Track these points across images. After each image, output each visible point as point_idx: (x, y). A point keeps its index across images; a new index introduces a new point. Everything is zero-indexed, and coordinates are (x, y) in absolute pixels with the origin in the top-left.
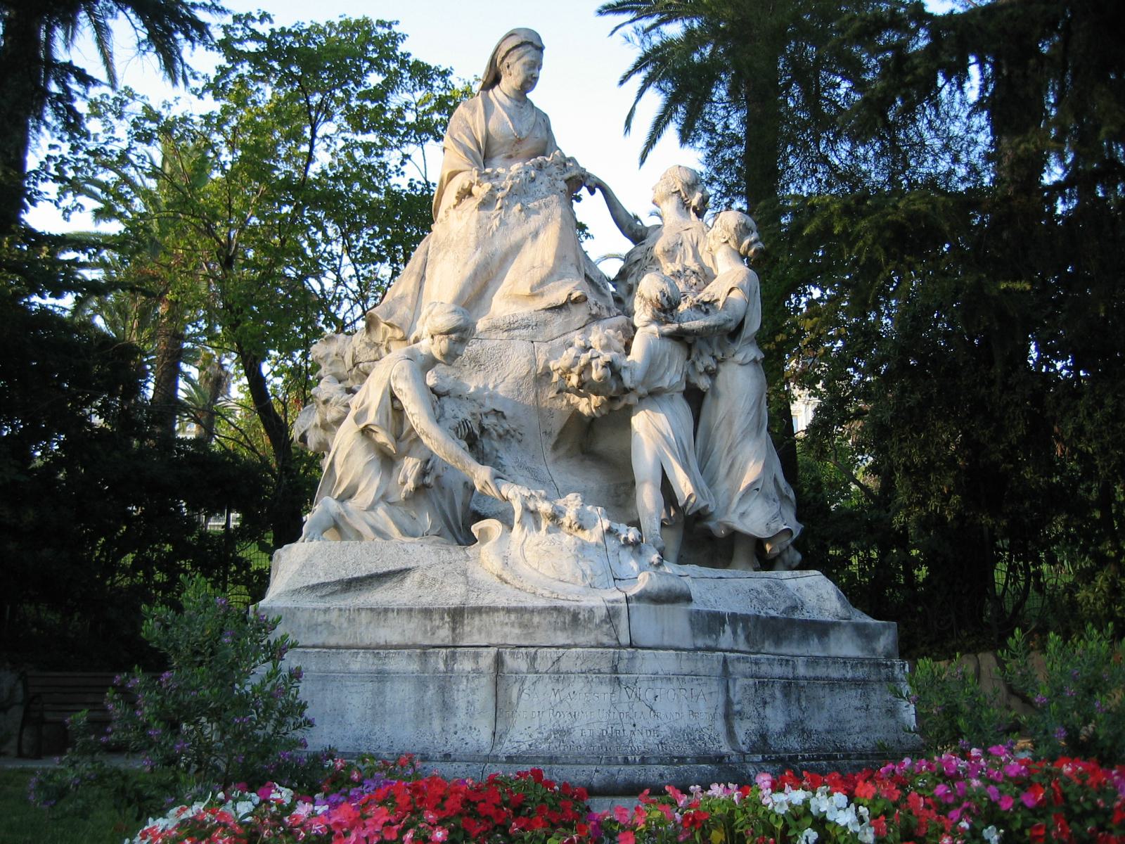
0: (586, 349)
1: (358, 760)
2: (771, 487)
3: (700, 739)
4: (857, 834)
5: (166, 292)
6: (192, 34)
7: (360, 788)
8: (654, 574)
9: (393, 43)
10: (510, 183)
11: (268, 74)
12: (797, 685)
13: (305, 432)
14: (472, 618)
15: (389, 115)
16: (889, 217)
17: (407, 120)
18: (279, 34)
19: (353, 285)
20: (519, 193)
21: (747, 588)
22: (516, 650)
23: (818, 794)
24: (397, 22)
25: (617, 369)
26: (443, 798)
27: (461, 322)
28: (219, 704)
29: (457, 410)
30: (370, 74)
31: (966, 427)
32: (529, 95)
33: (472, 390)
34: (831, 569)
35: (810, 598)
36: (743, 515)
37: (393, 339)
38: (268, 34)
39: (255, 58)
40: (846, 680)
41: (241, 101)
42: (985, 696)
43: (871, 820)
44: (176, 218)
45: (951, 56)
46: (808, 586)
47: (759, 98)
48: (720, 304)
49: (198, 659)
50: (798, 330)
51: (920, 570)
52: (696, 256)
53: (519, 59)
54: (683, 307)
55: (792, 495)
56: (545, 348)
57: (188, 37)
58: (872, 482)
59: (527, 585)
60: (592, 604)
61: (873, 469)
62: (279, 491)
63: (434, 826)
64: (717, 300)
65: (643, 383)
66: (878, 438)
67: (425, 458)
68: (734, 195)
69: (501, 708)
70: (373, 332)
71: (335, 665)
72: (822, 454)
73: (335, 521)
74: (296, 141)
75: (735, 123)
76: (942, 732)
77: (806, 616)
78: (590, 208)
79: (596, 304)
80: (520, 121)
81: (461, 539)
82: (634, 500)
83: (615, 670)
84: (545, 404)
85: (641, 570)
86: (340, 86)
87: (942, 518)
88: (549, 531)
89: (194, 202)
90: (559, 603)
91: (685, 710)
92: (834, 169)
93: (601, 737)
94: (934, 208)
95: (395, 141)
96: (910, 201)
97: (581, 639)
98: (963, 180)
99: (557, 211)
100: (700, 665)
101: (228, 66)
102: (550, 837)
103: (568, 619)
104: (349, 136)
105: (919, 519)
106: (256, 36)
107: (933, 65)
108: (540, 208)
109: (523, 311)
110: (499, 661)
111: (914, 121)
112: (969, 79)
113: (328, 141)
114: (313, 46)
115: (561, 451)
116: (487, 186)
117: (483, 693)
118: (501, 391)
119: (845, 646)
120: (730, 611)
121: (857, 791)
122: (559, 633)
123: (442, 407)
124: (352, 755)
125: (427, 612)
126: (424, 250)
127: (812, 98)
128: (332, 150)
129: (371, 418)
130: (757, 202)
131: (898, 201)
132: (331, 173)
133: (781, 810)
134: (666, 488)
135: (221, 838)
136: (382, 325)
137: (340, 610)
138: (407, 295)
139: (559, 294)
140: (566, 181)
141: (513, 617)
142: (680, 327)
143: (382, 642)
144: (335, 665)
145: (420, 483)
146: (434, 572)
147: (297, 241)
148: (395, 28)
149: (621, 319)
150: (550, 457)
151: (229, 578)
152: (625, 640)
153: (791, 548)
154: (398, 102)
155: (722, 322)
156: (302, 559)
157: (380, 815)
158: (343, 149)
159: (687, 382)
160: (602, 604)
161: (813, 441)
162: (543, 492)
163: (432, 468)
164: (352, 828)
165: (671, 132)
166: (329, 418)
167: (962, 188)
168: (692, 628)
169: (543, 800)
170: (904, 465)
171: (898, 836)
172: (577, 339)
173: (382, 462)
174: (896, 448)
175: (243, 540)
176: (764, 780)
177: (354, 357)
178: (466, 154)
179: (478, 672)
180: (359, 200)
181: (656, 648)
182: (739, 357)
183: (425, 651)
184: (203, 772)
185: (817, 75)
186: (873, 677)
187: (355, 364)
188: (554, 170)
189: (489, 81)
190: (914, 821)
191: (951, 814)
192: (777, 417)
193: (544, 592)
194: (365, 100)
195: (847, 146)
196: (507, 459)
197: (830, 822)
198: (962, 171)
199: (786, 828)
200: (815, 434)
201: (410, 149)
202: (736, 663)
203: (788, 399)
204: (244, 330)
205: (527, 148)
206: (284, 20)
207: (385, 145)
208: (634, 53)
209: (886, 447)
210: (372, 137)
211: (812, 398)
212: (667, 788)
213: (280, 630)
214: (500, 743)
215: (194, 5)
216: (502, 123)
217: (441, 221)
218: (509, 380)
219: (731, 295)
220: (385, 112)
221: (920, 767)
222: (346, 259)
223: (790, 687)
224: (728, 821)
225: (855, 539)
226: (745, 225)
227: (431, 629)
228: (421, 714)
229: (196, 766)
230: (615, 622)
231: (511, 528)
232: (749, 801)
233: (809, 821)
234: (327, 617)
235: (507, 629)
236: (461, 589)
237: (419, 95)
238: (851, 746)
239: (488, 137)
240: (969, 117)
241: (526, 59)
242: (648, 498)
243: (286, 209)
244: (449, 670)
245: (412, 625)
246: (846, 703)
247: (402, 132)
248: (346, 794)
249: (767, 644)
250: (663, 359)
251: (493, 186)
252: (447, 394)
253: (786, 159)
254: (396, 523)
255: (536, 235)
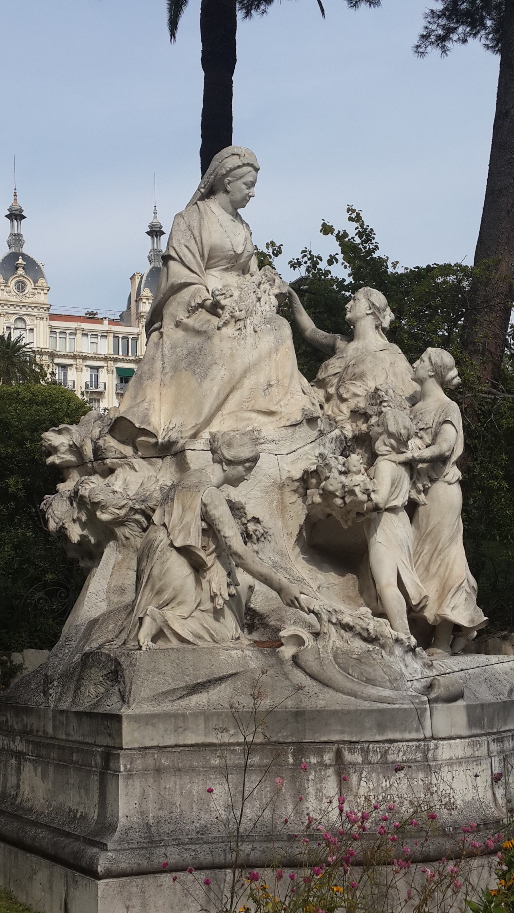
22: (352, 746)
71: (94, 749)
110: (339, 755)
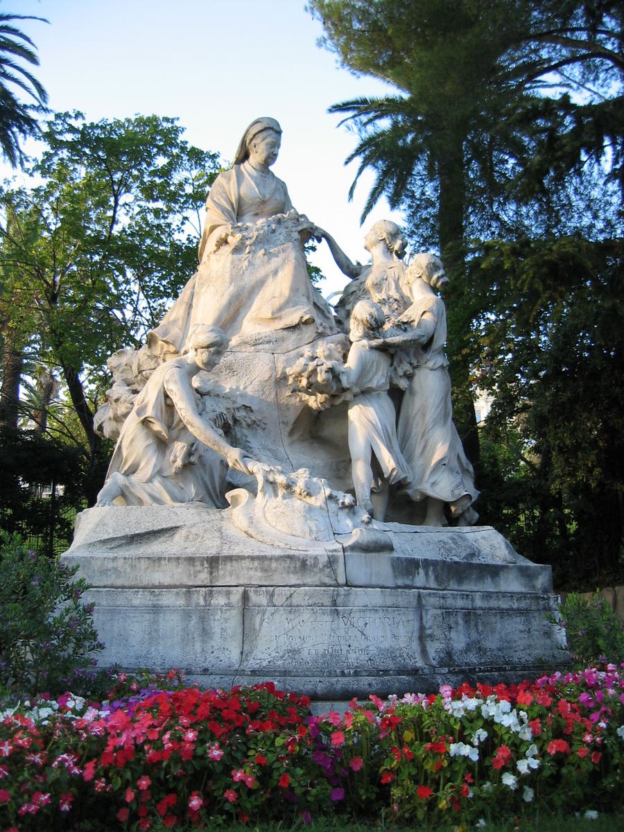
0: (313, 358)
1: (137, 674)
2: (455, 463)
3: (400, 656)
4: (518, 733)
5: (8, 320)
6: (24, 128)
7: (137, 696)
8: (364, 530)
9: (175, 134)
10: (256, 233)
11: (81, 157)
12: (475, 613)
13: (102, 423)
14: (225, 564)
15: (172, 188)
16: (546, 258)
17: (187, 192)
18: (89, 128)
19: (147, 315)
20: (262, 241)
21: (436, 540)
22: (258, 589)
23: (488, 702)
24: (178, 119)
25: (337, 373)
26: (197, 706)
27: (217, 339)
28: (27, 632)
29: (215, 406)
30: (158, 157)
31: (605, 417)
32: (271, 168)
33: (227, 390)
34: (502, 526)
35: (485, 548)
36: (434, 484)
37: (168, 352)
38: (81, 128)
39: (71, 146)
40: (512, 609)
41: (62, 178)
42: (619, 622)
43: (529, 722)
44: (15, 266)
45: (590, 137)
46: (483, 538)
47: (448, 171)
48: (415, 324)
49: (14, 597)
50: (479, 346)
51: (571, 524)
52: (398, 288)
53: (263, 140)
54: (387, 326)
55: (471, 469)
56: (283, 358)
57: (22, 131)
58: (536, 459)
59: (268, 539)
60: (316, 553)
61: (536, 449)
62: (84, 467)
63: (187, 728)
64: (413, 321)
65: (356, 384)
66: (539, 425)
67: (190, 443)
68: (430, 244)
69: (247, 633)
70: (153, 347)
71: (121, 600)
72: (497, 437)
73: (122, 491)
74: (104, 207)
75: (429, 191)
76: (586, 650)
77: (482, 561)
78: (320, 256)
79: (321, 325)
80: (264, 187)
81: (219, 504)
82: (351, 473)
83: (334, 604)
84: (283, 401)
85: (355, 527)
86: (134, 167)
87: (587, 486)
88: (284, 497)
89: (28, 254)
90: (291, 553)
91: (389, 634)
92: (503, 223)
93: (324, 656)
94: (580, 250)
95: (177, 207)
96: (561, 245)
97: (309, 580)
98: (601, 231)
99: (292, 254)
100: (400, 599)
101: (52, 152)
102: (278, 736)
103: (298, 564)
104: (142, 203)
105: (570, 486)
106: (72, 130)
107: (577, 144)
108: (279, 252)
109: (266, 330)
110: (245, 597)
111: (564, 187)
112: (604, 154)
113: (127, 207)
114: (115, 137)
115: (295, 437)
116: (239, 236)
117: (233, 621)
118: (249, 391)
119: (512, 584)
120: (423, 558)
121: (518, 698)
122: (291, 575)
123: (204, 404)
124: (133, 670)
125: (191, 560)
126: (191, 285)
127: (488, 170)
128: (130, 214)
129: (149, 412)
130: (447, 243)
131: (552, 245)
132: (129, 232)
133: (459, 715)
134: (375, 464)
135: (21, 739)
136: (160, 342)
137: (125, 558)
138: (179, 319)
139: (293, 317)
140: (300, 232)
141: (256, 563)
142: (385, 341)
143: (157, 584)
144: (121, 600)
145: (187, 462)
146: (196, 529)
147: (105, 282)
148: (177, 123)
149: (341, 336)
150: (286, 441)
151: (55, 534)
152: (342, 580)
153: (471, 509)
154: (179, 178)
155: (416, 337)
156: (97, 520)
157: (144, 718)
158: (138, 213)
159: (391, 383)
160: (325, 553)
161: (490, 428)
162: (280, 468)
163: (196, 450)
164: (123, 730)
165: (383, 201)
166: (119, 413)
167: (601, 238)
168: (394, 572)
169: (274, 706)
170: (559, 446)
171: (550, 734)
172: (307, 350)
173: (158, 446)
174: (552, 434)
175: (66, 505)
176: (446, 690)
177: (139, 366)
178: (223, 212)
179: (229, 605)
180: (150, 251)
181: (366, 587)
182: (430, 364)
183: (189, 588)
184: (18, 684)
185: (491, 154)
186: (534, 607)
187: (140, 372)
188: (290, 224)
189: (240, 158)
190: (563, 722)
191: (592, 716)
192: (464, 410)
193: (280, 544)
194: (154, 177)
195: (513, 207)
196: (254, 444)
197: (497, 724)
198: (600, 225)
199: (463, 728)
200: (492, 423)
201: (189, 213)
202: (427, 598)
203: (472, 398)
204: (65, 349)
205: (268, 208)
206: (92, 118)
207: (170, 210)
208: (354, 141)
209: (545, 433)
210: (160, 204)
211: (490, 397)
212: (371, 697)
213: (79, 575)
214: (247, 660)
215: (25, 106)
216: (250, 188)
217: (205, 263)
218: (256, 383)
219: (424, 317)
220: (169, 185)
221: (568, 679)
222: (142, 296)
223: (470, 615)
224: (418, 723)
225: (524, 501)
226: (434, 264)
227: (194, 573)
228: (186, 638)
229: (14, 680)
230: (335, 567)
231: (256, 495)
232: (435, 707)
233: (481, 723)
234: (115, 564)
235: (251, 573)
236: (217, 542)
237: (195, 173)
238: (517, 660)
239: (240, 200)
240: (605, 184)
241: (269, 140)
242: (361, 472)
243: (97, 258)
244: (208, 604)
245: (180, 570)
246: (513, 627)
247: (182, 200)
248: (126, 701)
249: (451, 583)
250: (372, 366)
251: (243, 236)
252: (208, 394)
253: (468, 218)
254: (169, 492)
255: (275, 273)
